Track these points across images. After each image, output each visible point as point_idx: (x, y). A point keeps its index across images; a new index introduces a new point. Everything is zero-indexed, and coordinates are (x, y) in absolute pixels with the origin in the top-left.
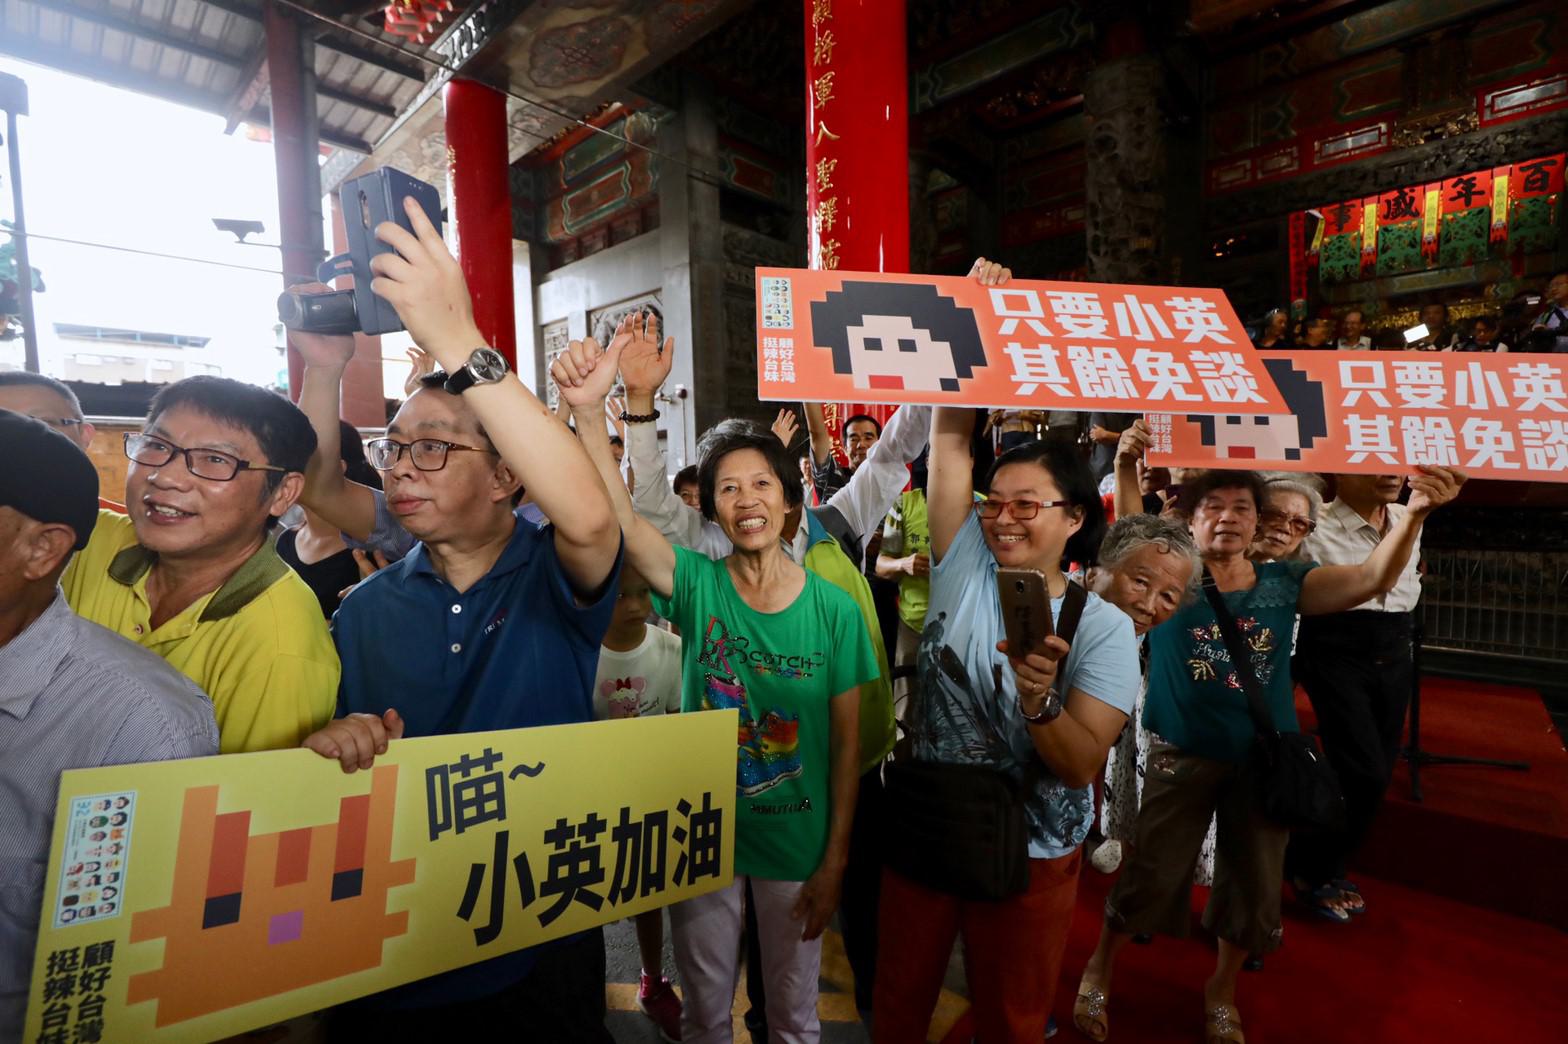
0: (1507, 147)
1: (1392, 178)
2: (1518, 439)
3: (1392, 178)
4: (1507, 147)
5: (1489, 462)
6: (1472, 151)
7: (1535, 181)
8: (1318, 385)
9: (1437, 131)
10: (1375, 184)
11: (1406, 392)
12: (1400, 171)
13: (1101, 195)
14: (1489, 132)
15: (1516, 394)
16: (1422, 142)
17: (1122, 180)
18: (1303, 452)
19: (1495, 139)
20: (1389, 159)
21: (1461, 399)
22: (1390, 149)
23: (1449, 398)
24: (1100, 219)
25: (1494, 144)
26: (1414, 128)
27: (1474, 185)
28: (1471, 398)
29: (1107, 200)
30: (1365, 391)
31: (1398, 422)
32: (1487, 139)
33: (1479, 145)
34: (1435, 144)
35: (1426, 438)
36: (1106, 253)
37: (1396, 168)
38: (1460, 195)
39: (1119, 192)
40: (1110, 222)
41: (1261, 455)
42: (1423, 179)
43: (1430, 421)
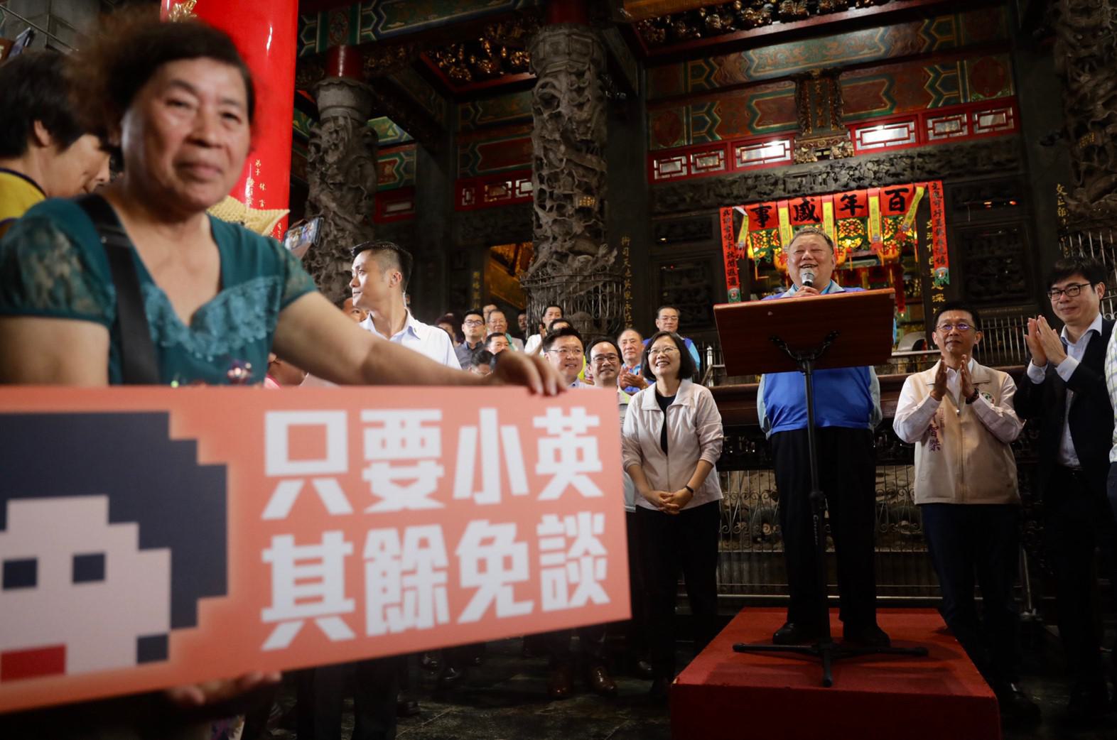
0: (875, 173)
1: (796, 186)
2: (534, 555)
3: (796, 186)
4: (875, 173)
5: (492, 607)
6: (851, 173)
7: (897, 203)
8: (218, 473)
9: (826, 153)
10: (784, 190)
11: (378, 478)
12: (802, 181)
13: (545, 149)
14: (862, 159)
15: (541, 469)
16: (816, 160)
17: (566, 137)
18: (178, 640)
19: (866, 165)
20: (794, 170)
21: (462, 488)
22: (793, 162)
23: (444, 488)
24: (545, 172)
25: (866, 169)
26: (809, 147)
27: (856, 201)
28: (478, 485)
29: (551, 155)
30: (308, 479)
31: (359, 544)
32: (860, 164)
33: (856, 169)
34: (826, 163)
35: (405, 573)
36: (551, 209)
37: (799, 179)
38: (847, 207)
39: (563, 148)
40: (554, 178)
41: (76, 665)
42: (819, 191)
43: (414, 534)
